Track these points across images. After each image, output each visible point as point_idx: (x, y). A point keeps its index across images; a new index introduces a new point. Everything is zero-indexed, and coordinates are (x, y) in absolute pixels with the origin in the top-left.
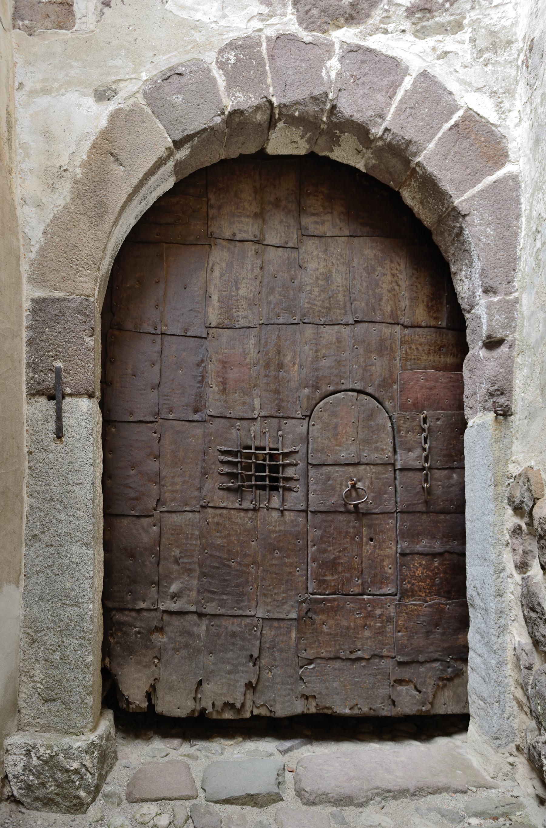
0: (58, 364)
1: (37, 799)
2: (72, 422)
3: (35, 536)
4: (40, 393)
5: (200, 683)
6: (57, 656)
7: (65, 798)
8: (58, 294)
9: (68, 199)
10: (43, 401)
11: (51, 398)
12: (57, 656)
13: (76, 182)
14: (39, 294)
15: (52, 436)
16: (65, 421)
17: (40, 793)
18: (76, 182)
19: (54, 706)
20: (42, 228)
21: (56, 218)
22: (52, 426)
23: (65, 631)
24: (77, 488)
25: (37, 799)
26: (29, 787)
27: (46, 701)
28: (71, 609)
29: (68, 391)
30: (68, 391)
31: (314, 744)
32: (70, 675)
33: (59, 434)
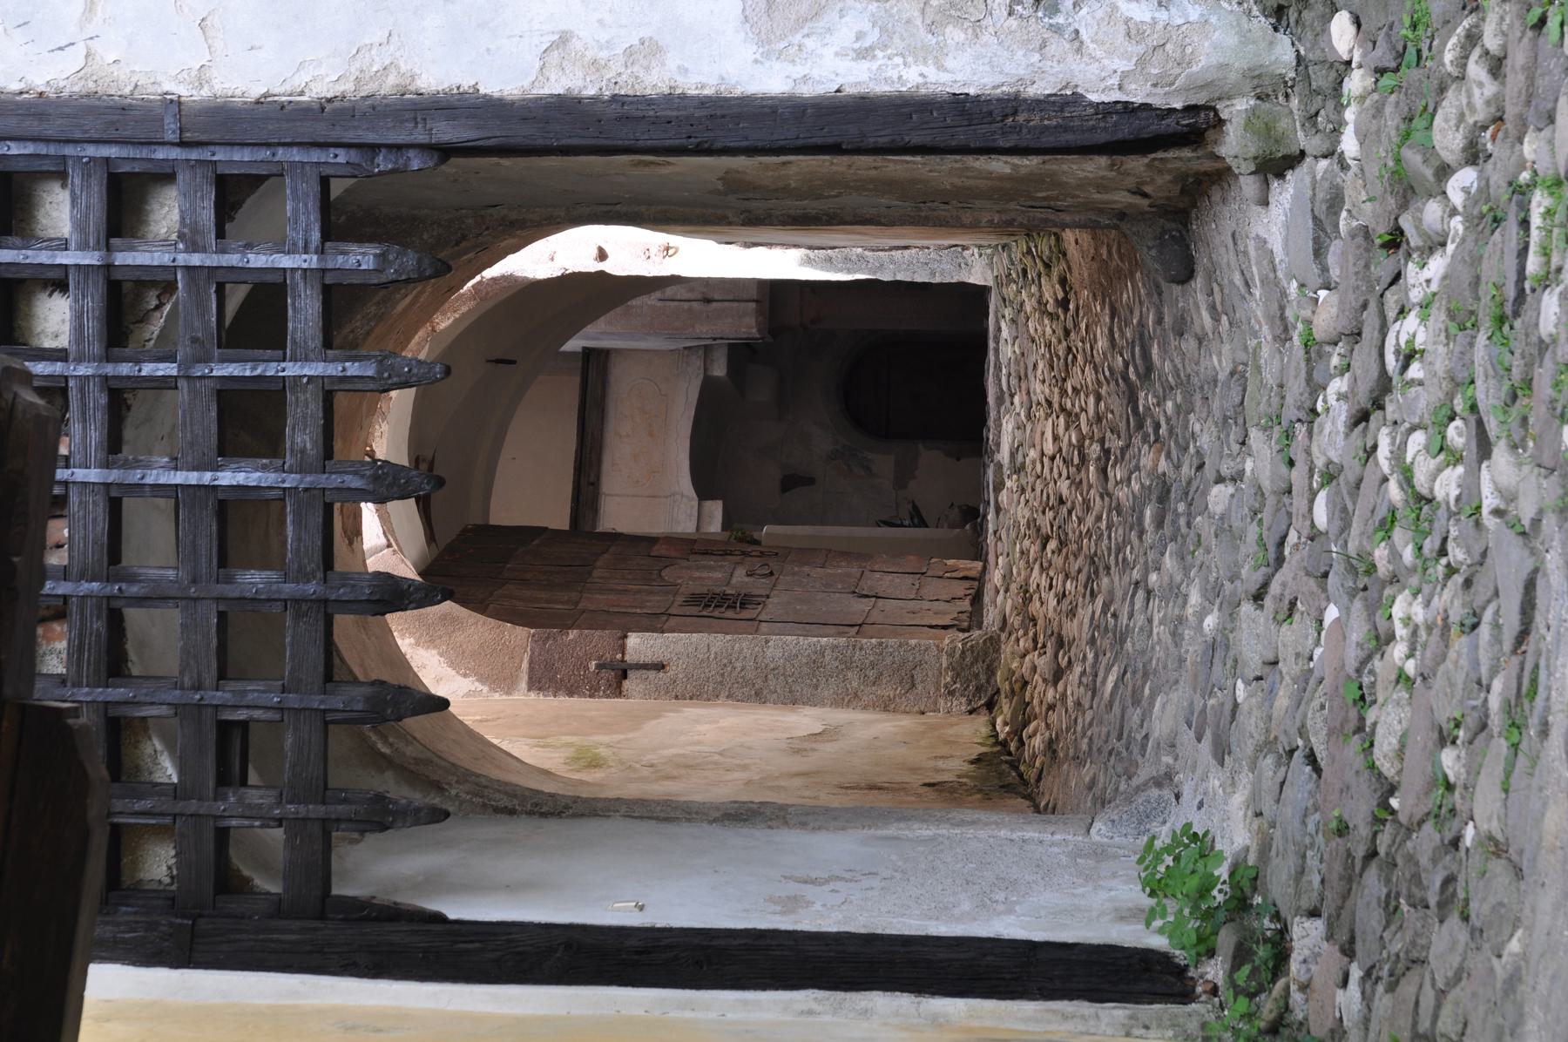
0: (593, 665)
1: (988, 682)
2: (650, 654)
3: (757, 694)
4: (619, 685)
5: (1317, 770)
6: (871, 673)
7: (986, 654)
8: (525, 665)
9: (434, 652)
10: (626, 684)
11: (625, 676)
12: (871, 673)
13: (417, 644)
14: (524, 685)
15: (661, 674)
16: (648, 660)
17: (983, 678)
18: (417, 644)
19: (918, 677)
20: (460, 678)
21: (452, 664)
22: (652, 674)
23: (848, 664)
24: (713, 650)
25: (988, 682)
26: (979, 689)
27: (913, 685)
28: (827, 658)
29: (619, 656)
30: (619, 656)
31: (23, 324)
32: (889, 660)
33: (660, 667)
